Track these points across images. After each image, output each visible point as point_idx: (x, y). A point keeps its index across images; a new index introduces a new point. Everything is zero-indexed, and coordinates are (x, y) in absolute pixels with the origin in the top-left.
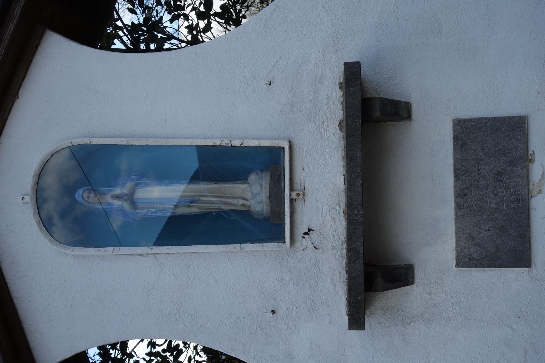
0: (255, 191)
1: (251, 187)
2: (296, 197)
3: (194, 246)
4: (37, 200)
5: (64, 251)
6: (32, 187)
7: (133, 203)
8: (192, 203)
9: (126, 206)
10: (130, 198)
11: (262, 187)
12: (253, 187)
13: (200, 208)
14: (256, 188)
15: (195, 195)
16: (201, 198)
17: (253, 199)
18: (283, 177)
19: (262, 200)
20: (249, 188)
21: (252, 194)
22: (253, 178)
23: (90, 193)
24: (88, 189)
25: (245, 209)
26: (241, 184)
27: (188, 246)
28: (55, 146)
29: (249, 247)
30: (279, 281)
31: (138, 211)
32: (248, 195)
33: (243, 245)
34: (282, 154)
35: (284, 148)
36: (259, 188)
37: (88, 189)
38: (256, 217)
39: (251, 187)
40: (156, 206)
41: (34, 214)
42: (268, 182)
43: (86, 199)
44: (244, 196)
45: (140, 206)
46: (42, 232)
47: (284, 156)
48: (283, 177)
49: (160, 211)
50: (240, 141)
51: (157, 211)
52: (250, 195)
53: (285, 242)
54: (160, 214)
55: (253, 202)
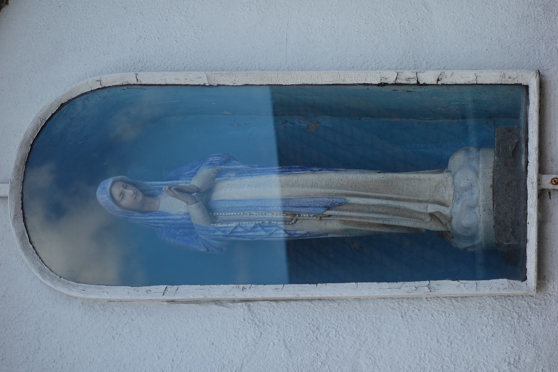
0: (464, 183)
1: (453, 176)
2: (551, 187)
3: (330, 286)
4: (22, 193)
5: (65, 291)
6: (16, 167)
7: (209, 210)
8: (328, 208)
9: (196, 213)
10: (204, 197)
11: (477, 174)
12: (458, 175)
13: (345, 222)
14: (464, 177)
15: (337, 194)
16: (348, 198)
17: (456, 200)
18: (523, 145)
19: (477, 200)
20: (450, 178)
21: (457, 193)
22: (458, 159)
23: (125, 188)
24: (122, 180)
25: (440, 228)
26: (434, 173)
27: (319, 285)
28: (69, 89)
29: (448, 287)
30: (509, 363)
31: (219, 225)
32: (447, 194)
33: (433, 283)
34: (523, 99)
35: (527, 87)
36: (471, 175)
37: (122, 180)
38: (462, 245)
39: (453, 176)
40: (255, 215)
41: (15, 218)
42: (491, 165)
43: (117, 197)
44: (438, 197)
45: (222, 215)
46: (26, 254)
47: (527, 103)
48: (523, 145)
49: (262, 226)
50: (438, 73)
51: (255, 227)
52: (452, 192)
53: (525, 279)
54: (263, 233)
55: (457, 208)
